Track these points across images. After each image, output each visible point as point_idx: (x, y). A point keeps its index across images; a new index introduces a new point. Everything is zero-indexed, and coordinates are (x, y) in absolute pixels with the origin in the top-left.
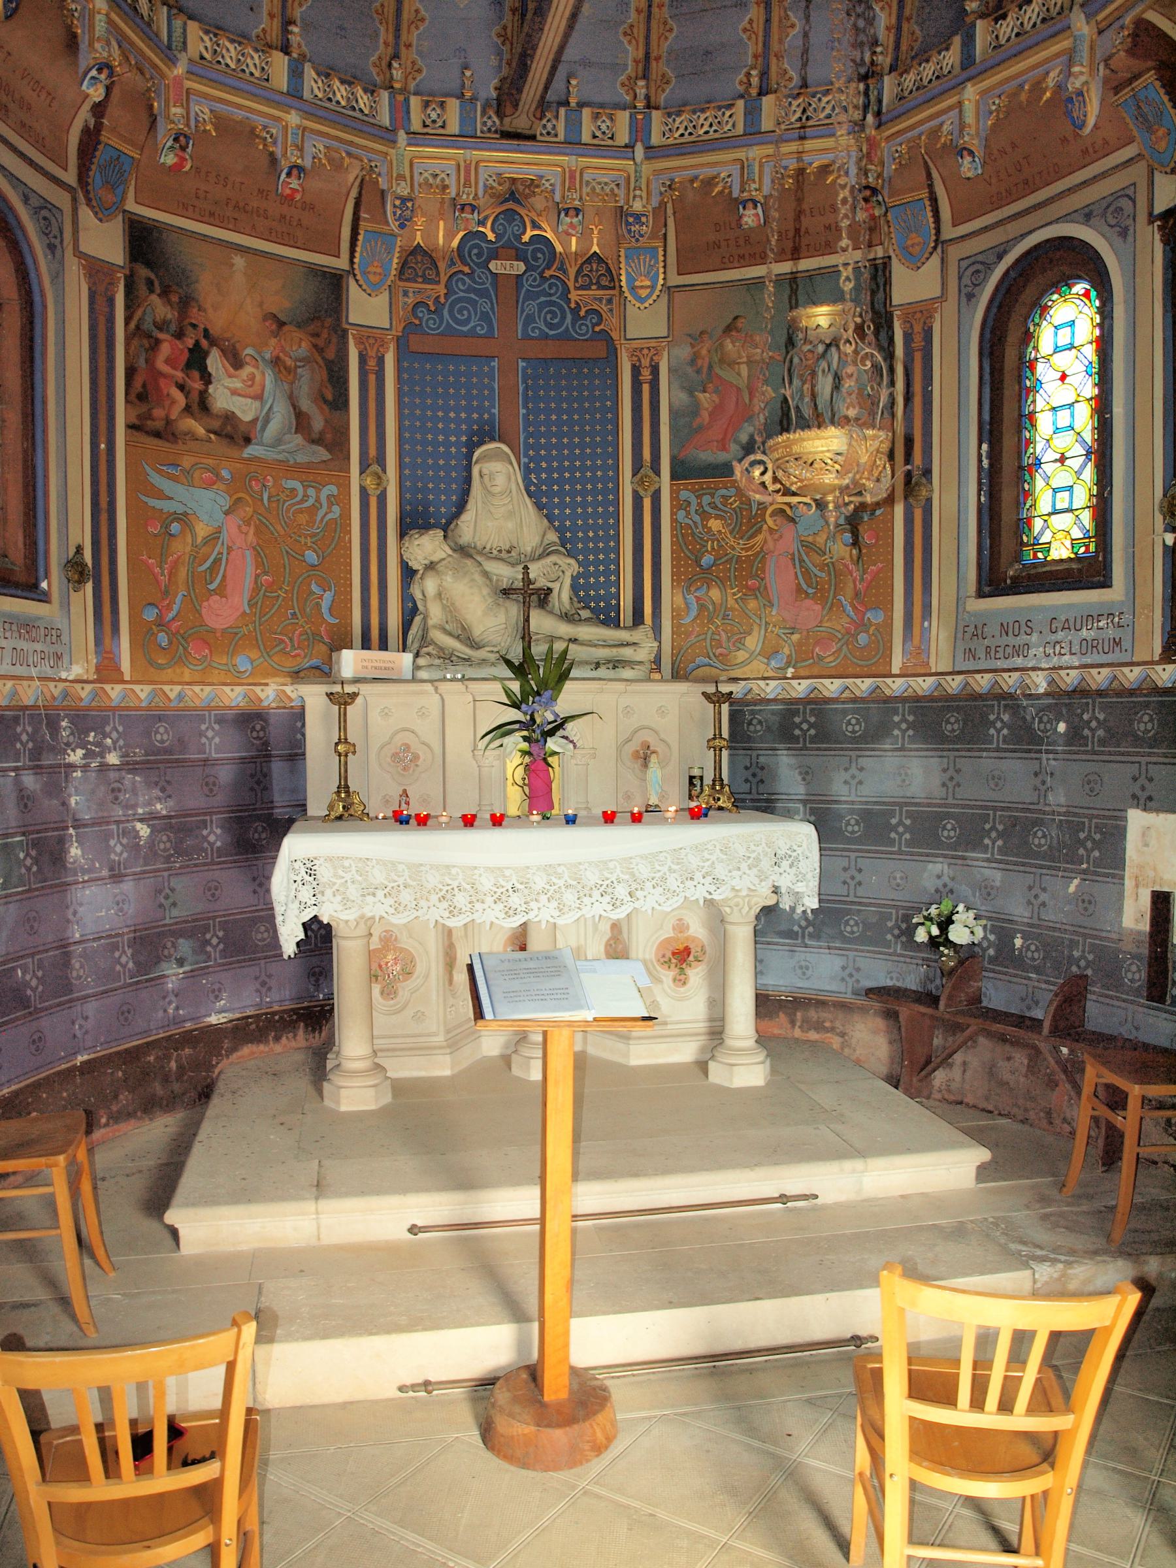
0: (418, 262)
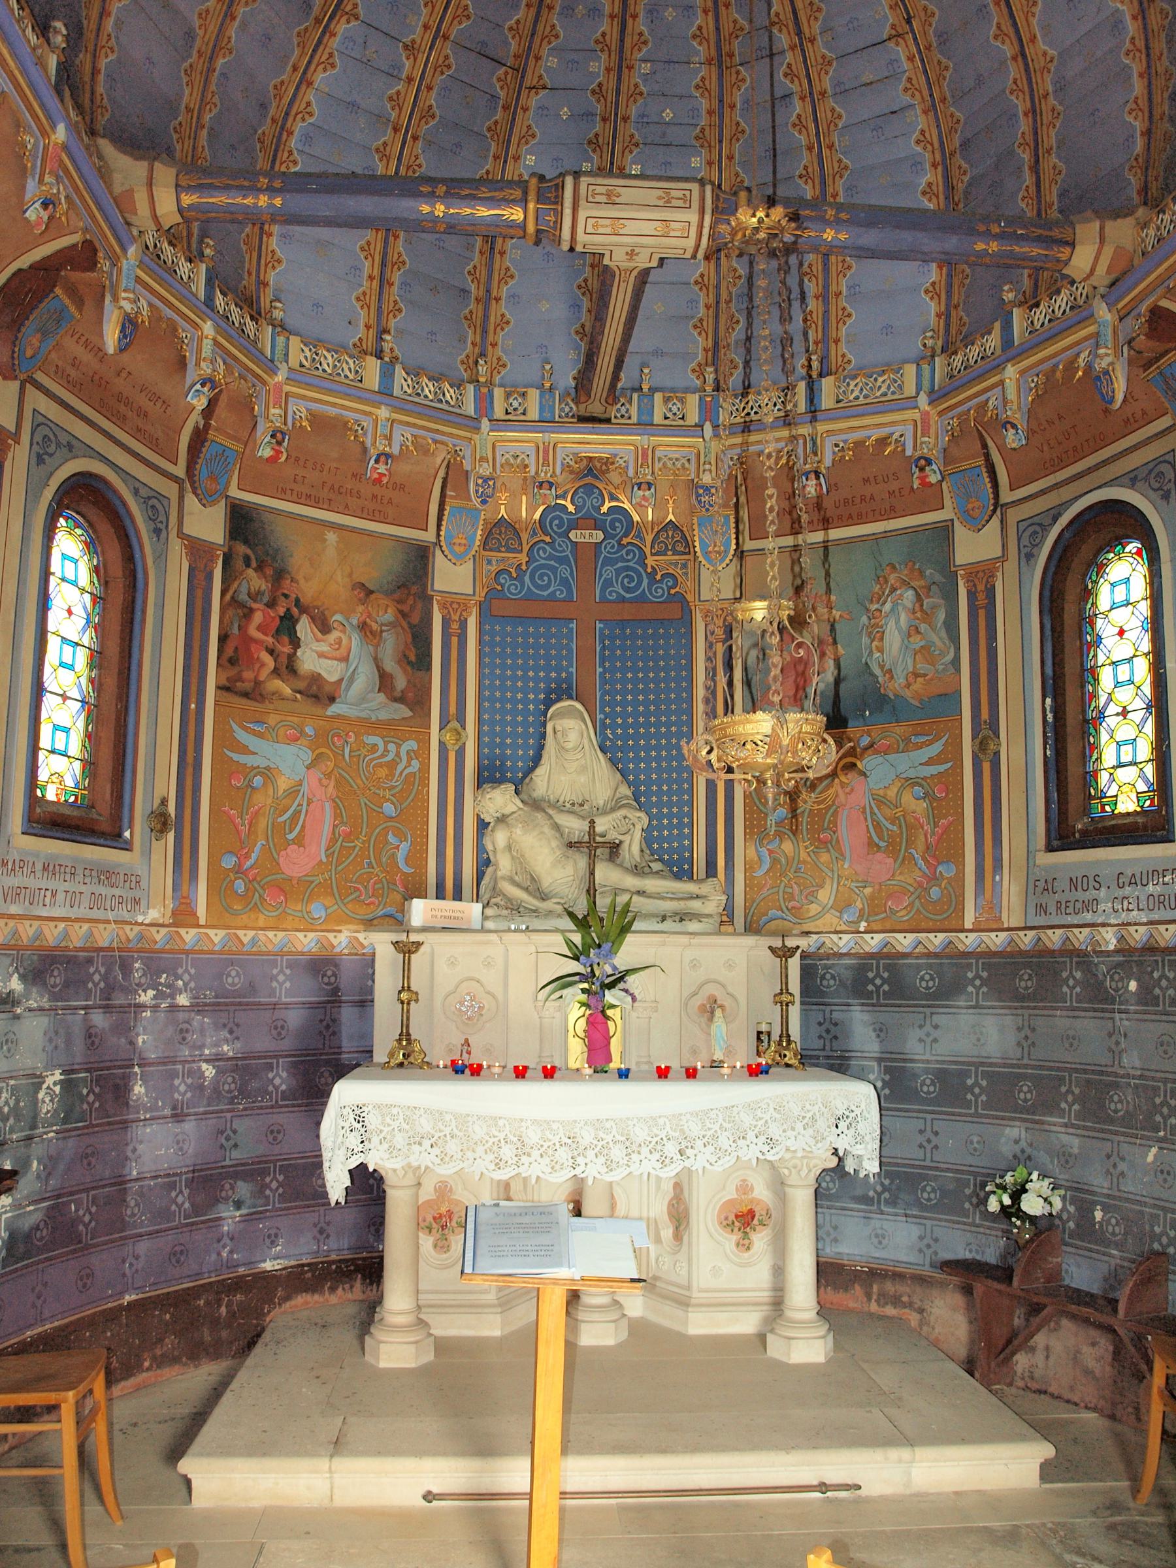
0: (500, 533)
